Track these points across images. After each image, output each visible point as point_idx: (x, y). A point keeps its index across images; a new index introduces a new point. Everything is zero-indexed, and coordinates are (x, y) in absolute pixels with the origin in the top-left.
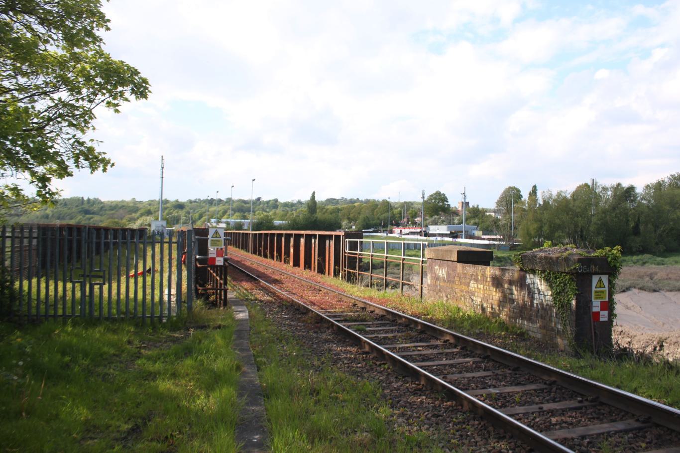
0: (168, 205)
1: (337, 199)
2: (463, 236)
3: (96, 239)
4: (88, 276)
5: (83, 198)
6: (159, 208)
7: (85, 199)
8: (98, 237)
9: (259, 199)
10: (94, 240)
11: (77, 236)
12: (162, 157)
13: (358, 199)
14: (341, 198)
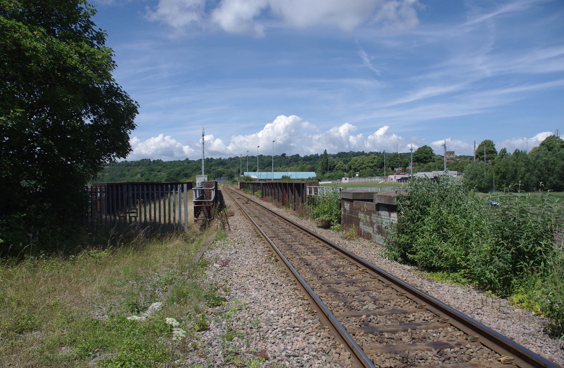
0: (213, 163)
1: (347, 152)
2: (203, 172)
3: (142, 191)
4: (128, 213)
5: (149, 159)
6: (274, 166)
7: (152, 160)
8: (117, 190)
9: (284, 155)
10: (141, 192)
11: (147, 191)
12: (475, 142)
13: (363, 152)
14: (349, 152)
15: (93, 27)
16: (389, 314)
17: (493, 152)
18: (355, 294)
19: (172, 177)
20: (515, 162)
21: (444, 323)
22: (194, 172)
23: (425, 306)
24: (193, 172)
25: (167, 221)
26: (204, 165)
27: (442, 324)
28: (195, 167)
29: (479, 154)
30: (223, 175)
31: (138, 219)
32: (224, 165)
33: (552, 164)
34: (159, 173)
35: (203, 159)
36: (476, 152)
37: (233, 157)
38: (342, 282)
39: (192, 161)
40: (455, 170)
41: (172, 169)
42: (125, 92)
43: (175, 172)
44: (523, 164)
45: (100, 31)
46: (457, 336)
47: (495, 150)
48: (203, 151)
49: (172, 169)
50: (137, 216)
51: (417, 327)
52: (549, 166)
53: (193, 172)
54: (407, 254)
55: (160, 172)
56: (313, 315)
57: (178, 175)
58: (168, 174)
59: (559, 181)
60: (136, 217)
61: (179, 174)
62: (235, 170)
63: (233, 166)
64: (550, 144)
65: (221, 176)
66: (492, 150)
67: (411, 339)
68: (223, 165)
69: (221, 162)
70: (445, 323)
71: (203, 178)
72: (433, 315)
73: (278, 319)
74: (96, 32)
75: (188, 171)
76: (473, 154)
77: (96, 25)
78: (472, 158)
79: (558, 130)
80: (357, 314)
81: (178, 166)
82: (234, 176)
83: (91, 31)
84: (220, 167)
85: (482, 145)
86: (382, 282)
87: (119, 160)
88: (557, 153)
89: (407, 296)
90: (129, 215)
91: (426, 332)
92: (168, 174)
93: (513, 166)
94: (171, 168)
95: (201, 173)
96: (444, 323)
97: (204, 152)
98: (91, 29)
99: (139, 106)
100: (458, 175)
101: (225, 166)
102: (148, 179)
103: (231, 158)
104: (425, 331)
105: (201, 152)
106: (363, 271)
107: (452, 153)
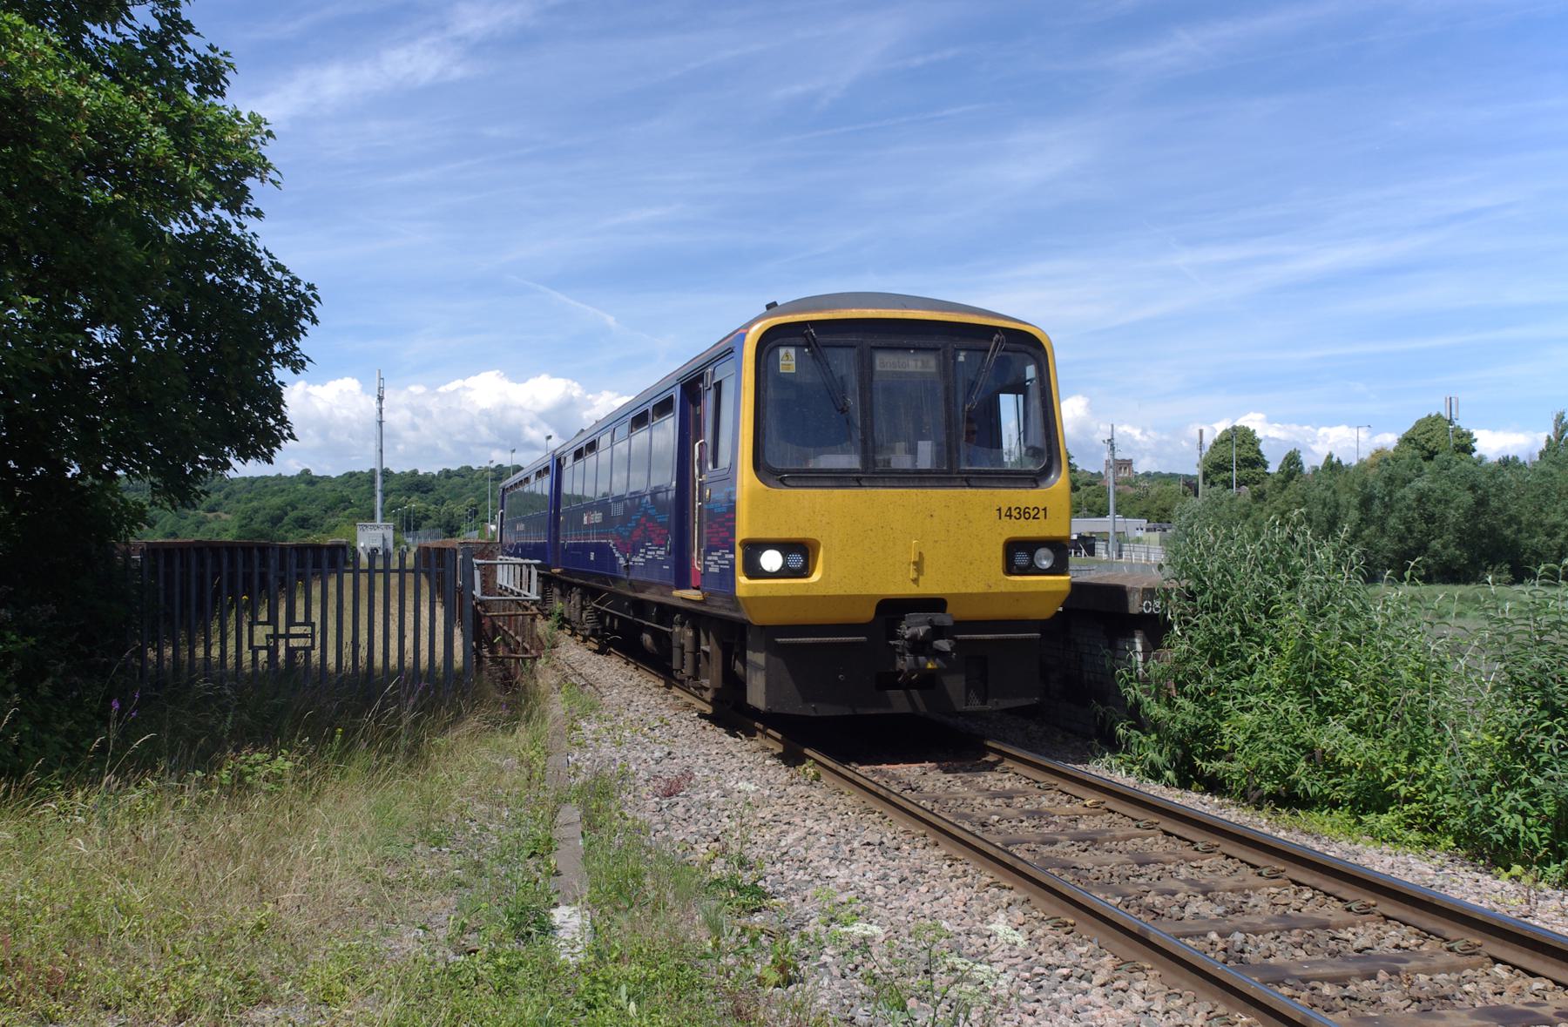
4: (282, 636)
10: (256, 571)
11: (438, 565)
15: (189, 39)
16: (1281, 931)
17: (1255, 461)
18: (1131, 873)
19: (255, 526)
20: (1329, 493)
21: (1471, 954)
22: (330, 513)
23: (1377, 908)
24: (326, 511)
25: (393, 660)
26: (381, 491)
27: (1467, 957)
28: (331, 496)
29: (1216, 468)
30: (424, 523)
31: (316, 653)
32: (426, 492)
33: (1439, 502)
34: (211, 515)
35: (379, 472)
36: (1205, 461)
37: (454, 467)
38: (1060, 838)
39: (322, 478)
40: (1141, 515)
41: (255, 504)
42: (266, 252)
43: (267, 511)
44: (1355, 501)
45: (211, 54)
46: (1537, 993)
47: (1262, 456)
48: (378, 448)
49: (255, 504)
50: (313, 647)
51: (1400, 965)
52: (1430, 507)
53: (326, 511)
54: (1198, 762)
55: (214, 511)
56: (1067, 933)
57: (276, 520)
58: (244, 518)
59: (1458, 552)
60: (308, 650)
61: (280, 519)
62: (459, 509)
63: (457, 497)
64: (1428, 440)
65: (417, 528)
66: (1252, 455)
67: (1409, 1002)
68: (422, 492)
69: (418, 484)
70: (1473, 954)
71: (380, 532)
72: (1418, 934)
73: (985, 945)
74: (198, 56)
75: (313, 510)
76: (1195, 471)
77: (198, 34)
78: (1190, 485)
79: (1453, 400)
80: (1189, 930)
81: (274, 494)
82: (459, 528)
83: (178, 49)
84: (414, 498)
85: (1222, 442)
86: (1179, 838)
87: (250, 469)
88: (1453, 470)
89: (1296, 878)
90: (287, 643)
91: (1431, 980)
92: (244, 518)
93: (1325, 505)
94: (251, 500)
95: (372, 517)
96: (1471, 954)
97: (381, 451)
98: (179, 45)
99: (318, 298)
100: (1148, 530)
101: (431, 496)
102: (174, 534)
103: (448, 471)
104: (1428, 977)
105: (373, 446)
106: (1097, 806)
107: (1127, 464)
